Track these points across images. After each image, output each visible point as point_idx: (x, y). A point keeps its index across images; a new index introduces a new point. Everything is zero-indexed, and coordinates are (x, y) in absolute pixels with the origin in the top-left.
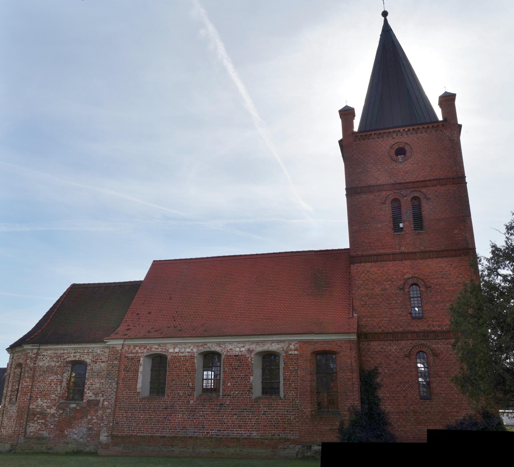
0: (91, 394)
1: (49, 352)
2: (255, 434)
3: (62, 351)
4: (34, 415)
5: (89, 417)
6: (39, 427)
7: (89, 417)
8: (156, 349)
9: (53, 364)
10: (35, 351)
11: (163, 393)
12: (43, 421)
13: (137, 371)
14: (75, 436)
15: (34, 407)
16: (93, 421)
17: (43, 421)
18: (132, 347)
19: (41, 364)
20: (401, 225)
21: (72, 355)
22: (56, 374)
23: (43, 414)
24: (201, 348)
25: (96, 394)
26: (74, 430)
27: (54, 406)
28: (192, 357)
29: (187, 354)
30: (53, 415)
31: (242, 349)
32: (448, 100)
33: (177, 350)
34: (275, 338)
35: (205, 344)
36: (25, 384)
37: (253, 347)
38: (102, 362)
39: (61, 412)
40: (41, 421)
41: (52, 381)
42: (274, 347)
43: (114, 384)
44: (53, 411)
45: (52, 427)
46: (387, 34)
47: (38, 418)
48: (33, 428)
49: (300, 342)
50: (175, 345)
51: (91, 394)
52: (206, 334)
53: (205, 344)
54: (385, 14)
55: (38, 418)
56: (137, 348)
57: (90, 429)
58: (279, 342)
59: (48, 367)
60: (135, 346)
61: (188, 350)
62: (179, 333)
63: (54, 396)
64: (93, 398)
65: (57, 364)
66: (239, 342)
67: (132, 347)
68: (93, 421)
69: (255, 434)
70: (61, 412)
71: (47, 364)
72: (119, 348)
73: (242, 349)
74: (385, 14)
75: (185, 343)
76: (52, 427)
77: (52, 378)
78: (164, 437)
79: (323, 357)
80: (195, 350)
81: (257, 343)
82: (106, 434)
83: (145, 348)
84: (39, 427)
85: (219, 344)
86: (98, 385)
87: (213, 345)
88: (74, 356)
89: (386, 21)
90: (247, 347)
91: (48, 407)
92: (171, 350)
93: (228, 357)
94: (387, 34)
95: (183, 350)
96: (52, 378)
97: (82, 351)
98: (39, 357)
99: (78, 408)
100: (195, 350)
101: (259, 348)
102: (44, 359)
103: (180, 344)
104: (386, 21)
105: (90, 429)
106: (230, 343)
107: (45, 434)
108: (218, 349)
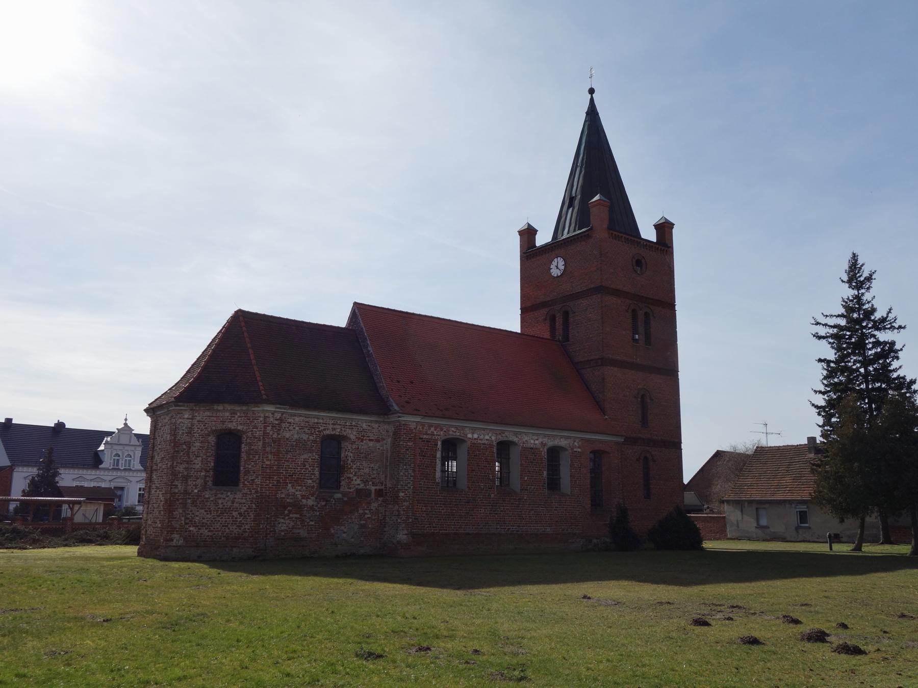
0: (358, 482)
1: (297, 419)
2: (548, 529)
3: (316, 420)
4: (285, 508)
5: (361, 511)
6: (292, 524)
7: (361, 511)
8: (453, 433)
9: (305, 437)
10: (278, 416)
11: (237, 484)
12: (298, 516)
13: (435, 457)
14: (345, 535)
15: (283, 496)
16: (367, 516)
17: (298, 516)
18: (426, 427)
19: (287, 435)
20: (637, 337)
21: (331, 426)
22: (311, 451)
23: (297, 506)
24: (499, 437)
25: (365, 482)
26: (343, 528)
27: (313, 495)
28: (491, 446)
29: (486, 442)
30: (312, 508)
31: (537, 442)
32: (664, 228)
33: (476, 436)
34: (566, 434)
35: (503, 432)
36: (268, 463)
37: (545, 440)
38: (370, 440)
39: (323, 503)
40: (295, 516)
41: (305, 460)
42: (563, 443)
43: (410, 471)
44: (310, 502)
45: (312, 523)
46: (592, 115)
47: (290, 511)
48: (284, 525)
49: (582, 439)
50: (474, 430)
51: (358, 482)
52: (503, 420)
53: (503, 432)
54: (592, 91)
55: (290, 511)
56: (432, 429)
57: (363, 526)
58: (567, 438)
59: (298, 441)
60: (430, 426)
61: (487, 437)
62: (472, 416)
63: (310, 481)
64: (362, 486)
65: (311, 438)
66: (534, 434)
67: (426, 427)
68: (367, 516)
69: (548, 529)
70: (323, 503)
71: (296, 436)
72: (413, 426)
73: (537, 442)
74: (592, 91)
75: (484, 429)
76: (312, 523)
77: (306, 456)
78: (468, 534)
79: (598, 455)
80: (493, 438)
81: (549, 436)
82: (405, 532)
83: (442, 430)
84: (292, 524)
85: (516, 434)
86: (367, 471)
87: (510, 434)
88: (334, 429)
89: (592, 100)
90: (540, 440)
91: (303, 497)
92: (470, 436)
93: (524, 449)
94: (592, 115)
95: (482, 437)
96: (306, 456)
97: (342, 422)
98: (283, 425)
99: (346, 499)
100: (493, 438)
101: (551, 443)
102: (291, 428)
103: (484, 429)
104: (592, 100)
105: (363, 526)
106: (526, 434)
107: (303, 533)
108: (515, 439)
